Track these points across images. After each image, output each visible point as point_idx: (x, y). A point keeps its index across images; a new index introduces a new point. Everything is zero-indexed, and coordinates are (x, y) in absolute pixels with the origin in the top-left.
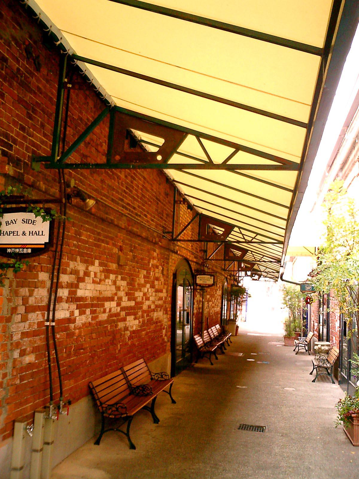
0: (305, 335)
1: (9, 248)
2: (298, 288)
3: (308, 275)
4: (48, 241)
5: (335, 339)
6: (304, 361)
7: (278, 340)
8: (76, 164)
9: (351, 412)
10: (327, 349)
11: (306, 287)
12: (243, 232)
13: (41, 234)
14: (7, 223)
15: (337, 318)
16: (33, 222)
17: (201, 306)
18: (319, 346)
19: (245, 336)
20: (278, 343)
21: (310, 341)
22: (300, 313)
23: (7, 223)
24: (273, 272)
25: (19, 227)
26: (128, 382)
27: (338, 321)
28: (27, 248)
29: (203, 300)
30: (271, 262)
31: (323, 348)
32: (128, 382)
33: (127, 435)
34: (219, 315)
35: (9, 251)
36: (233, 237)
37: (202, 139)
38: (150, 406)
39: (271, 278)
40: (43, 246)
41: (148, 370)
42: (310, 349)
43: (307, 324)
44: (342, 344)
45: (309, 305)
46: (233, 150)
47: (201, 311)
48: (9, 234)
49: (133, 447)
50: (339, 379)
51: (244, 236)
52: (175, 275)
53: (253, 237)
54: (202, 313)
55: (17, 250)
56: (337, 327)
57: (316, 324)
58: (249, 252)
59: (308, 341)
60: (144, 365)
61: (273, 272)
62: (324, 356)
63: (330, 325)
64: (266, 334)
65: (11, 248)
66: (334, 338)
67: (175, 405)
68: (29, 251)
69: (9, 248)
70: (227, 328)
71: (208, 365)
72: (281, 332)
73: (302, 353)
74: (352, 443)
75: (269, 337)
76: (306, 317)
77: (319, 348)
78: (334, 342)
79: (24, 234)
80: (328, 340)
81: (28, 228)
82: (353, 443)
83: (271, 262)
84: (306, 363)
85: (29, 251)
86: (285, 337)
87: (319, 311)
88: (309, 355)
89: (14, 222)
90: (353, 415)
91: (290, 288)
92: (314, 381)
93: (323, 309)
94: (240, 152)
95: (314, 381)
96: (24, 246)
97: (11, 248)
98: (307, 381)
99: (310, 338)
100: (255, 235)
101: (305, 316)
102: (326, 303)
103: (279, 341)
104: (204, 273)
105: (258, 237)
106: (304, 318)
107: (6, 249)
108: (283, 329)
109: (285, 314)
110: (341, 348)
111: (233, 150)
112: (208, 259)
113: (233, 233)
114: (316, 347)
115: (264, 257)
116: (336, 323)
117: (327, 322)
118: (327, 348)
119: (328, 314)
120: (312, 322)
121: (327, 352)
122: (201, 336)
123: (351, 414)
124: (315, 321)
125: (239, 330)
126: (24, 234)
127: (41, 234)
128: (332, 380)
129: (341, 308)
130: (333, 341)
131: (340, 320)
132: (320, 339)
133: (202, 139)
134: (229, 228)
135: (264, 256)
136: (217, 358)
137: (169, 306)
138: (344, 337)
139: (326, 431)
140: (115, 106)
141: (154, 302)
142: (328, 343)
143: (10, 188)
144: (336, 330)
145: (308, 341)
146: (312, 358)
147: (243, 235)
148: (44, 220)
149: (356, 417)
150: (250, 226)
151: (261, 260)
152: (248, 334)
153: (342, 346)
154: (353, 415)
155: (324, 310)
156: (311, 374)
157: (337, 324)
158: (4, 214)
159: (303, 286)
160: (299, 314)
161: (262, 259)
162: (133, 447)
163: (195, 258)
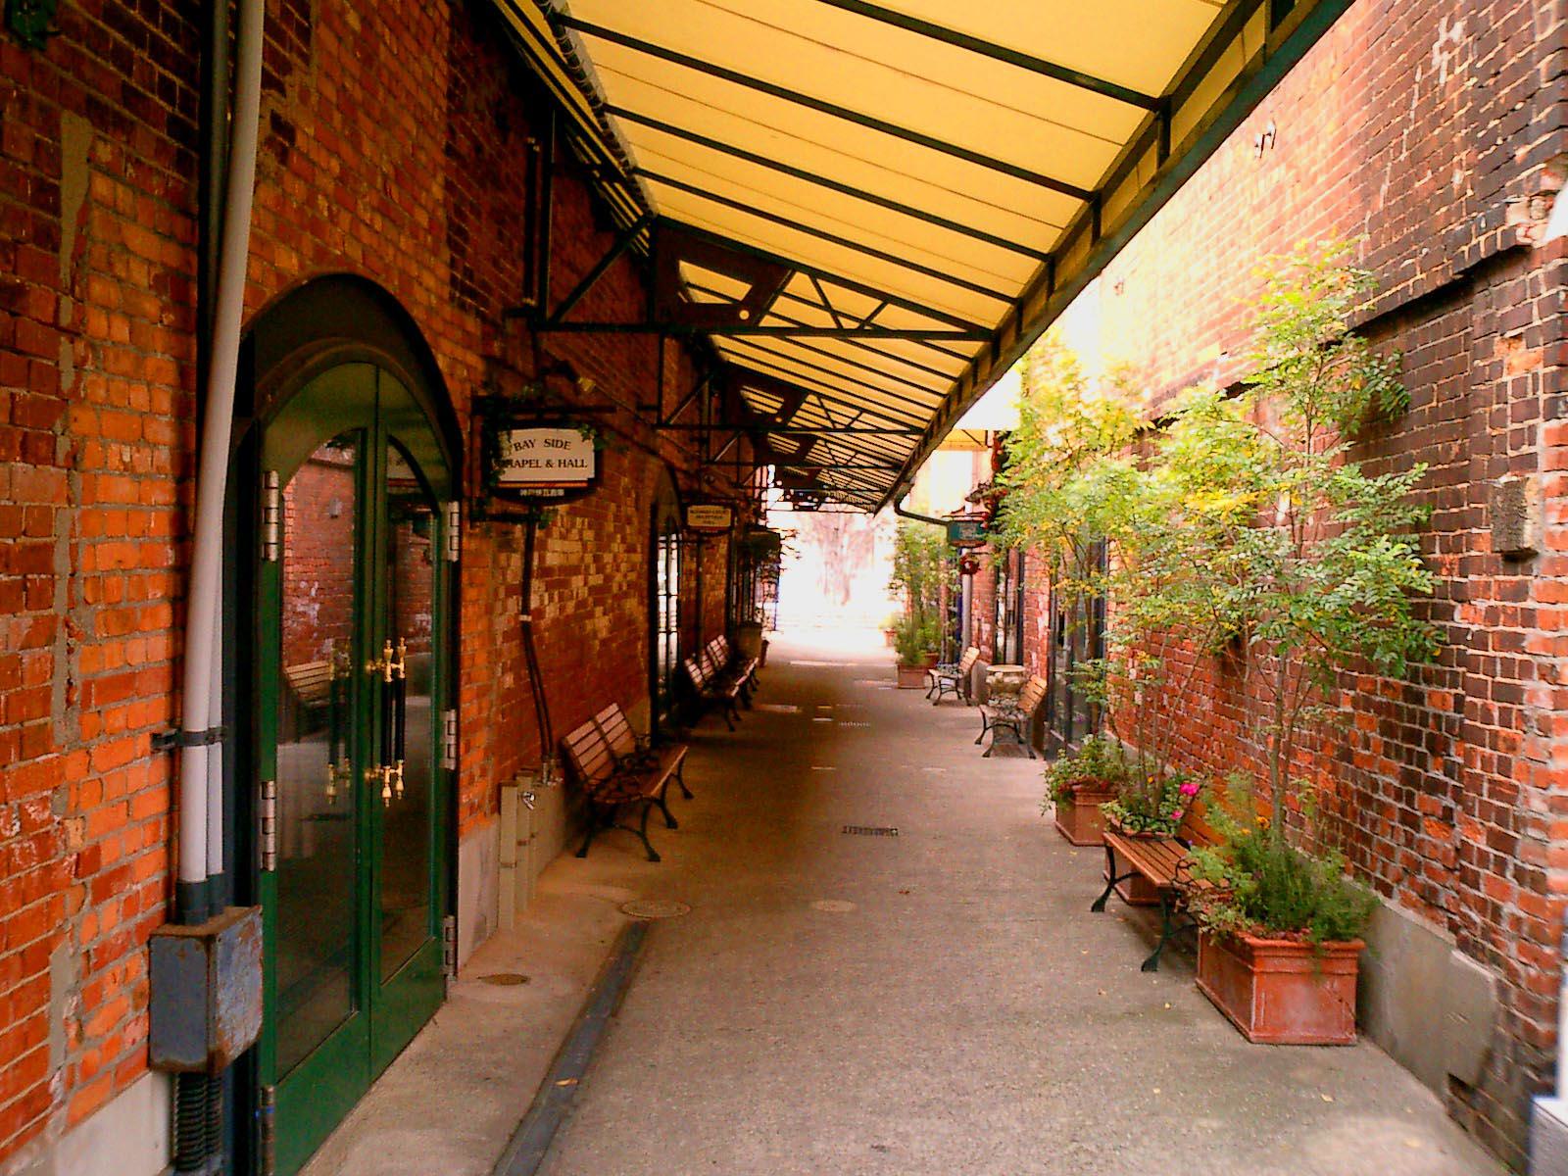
0: (956, 658)
1: (524, 488)
2: (940, 533)
3: (967, 499)
4: (592, 476)
5: (1037, 659)
6: (954, 719)
7: (880, 674)
8: (587, 324)
9: (1071, 781)
10: (1017, 682)
11: (961, 530)
12: (827, 404)
13: (579, 464)
14: (518, 446)
15: (1043, 600)
16: (565, 445)
17: (693, 584)
18: (999, 675)
19: (783, 667)
20: (879, 682)
21: (970, 671)
22: (937, 600)
23: (518, 446)
24: (869, 490)
25: (540, 453)
26: (608, 747)
27: (1046, 615)
28: (557, 488)
29: (701, 570)
30: (876, 467)
31: (1007, 680)
32: (608, 747)
33: (642, 835)
34: (723, 611)
35: (524, 493)
36: (807, 416)
37: (821, 283)
38: (658, 797)
39: (856, 504)
40: (585, 485)
41: (629, 727)
42: (971, 690)
43: (961, 628)
44: (1054, 669)
45: (966, 577)
46: (878, 303)
47: (693, 597)
48: (522, 464)
49: (654, 857)
50: (1045, 747)
51: (830, 414)
52: (654, 510)
53: (853, 416)
54: (698, 601)
55: (539, 492)
56: (1040, 627)
57: (986, 627)
58: (819, 442)
59: (965, 671)
60: (620, 716)
61: (869, 490)
62: (1009, 701)
63: (1025, 625)
64: (842, 661)
65: (527, 489)
66: (1034, 655)
67: (693, 800)
68: (561, 493)
69: (524, 488)
70: (746, 644)
71: (720, 732)
72: (885, 654)
73: (950, 703)
74: (1071, 842)
75: (851, 669)
76: (956, 609)
77: (998, 681)
78: (1035, 666)
79: (549, 464)
80: (1019, 661)
81: (556, 454)
82: (1075, 841)
83: (876, 467)
84: (967, 724)
85: (561, 493)
86: (901, 666)
87: (995, 592)
88: (969, 705)
89: (529, 444)
90: (1075, 787)
91: (916, 530)
92: (986, 755)
93: (1006, 586)
94: (890, 306)
95: (986, 755)
96: (551, 485)
97: (527, 489)
98: (972, 755)
99: (971, 663)
100: (857, 412)
101: (952, 608)
102: (1015, 571)
103: (882, 679)
104: (707, 500)
105: (865, 417)
106: (951, 614)
107: (519, 489)
108: (889, 645)
109: (895, 607)
110: (1050, 676)
111: (878, 303)
112: (712, 462)
113: (804, 406)
114: (990, 680)
115: (859, 456)
116: (1039, 620)
117: (1016, 620)
118: (1016, 680)
119: (1020, 595)
120: (975, 624)
121: (1017, 691)
122: (697, 662)
123: (1071, 786)
124: (983, 619)
125: (768, 649)
126: (549, 464)
127: (579, 464)
128: (1030, 753)
129: (1054, 580)
130: (1031, 664)
131: (1050, 610)
132: (997, 659)
133: (821, 283)
134: (793, 396)
135: (857, 452)
136: (737, 718)
137: (644, 584)
138: (1058, 647)
139: (1024, 831)
140: (659, 216)
141: (625, 576)
142: (1019, 668)
143: (526, 388)
144: (1040, 636)
145: (965, 671)
146: (974, 713)
147: (827, 410)
148: (585, 437)
149: (1081, 791)
150: (804, 367)
151: (850, 464)
152: (792, 663)
153: (1054, 673)
154: (1075, 787)
155: (1008, 588)
156: (979, 742)
157: (1043, 621)
158: (514, 432)
159: (953, 526)
160: (934, 603)
161: (854, 460)
162: (654, 857)
163: (686, 460)
